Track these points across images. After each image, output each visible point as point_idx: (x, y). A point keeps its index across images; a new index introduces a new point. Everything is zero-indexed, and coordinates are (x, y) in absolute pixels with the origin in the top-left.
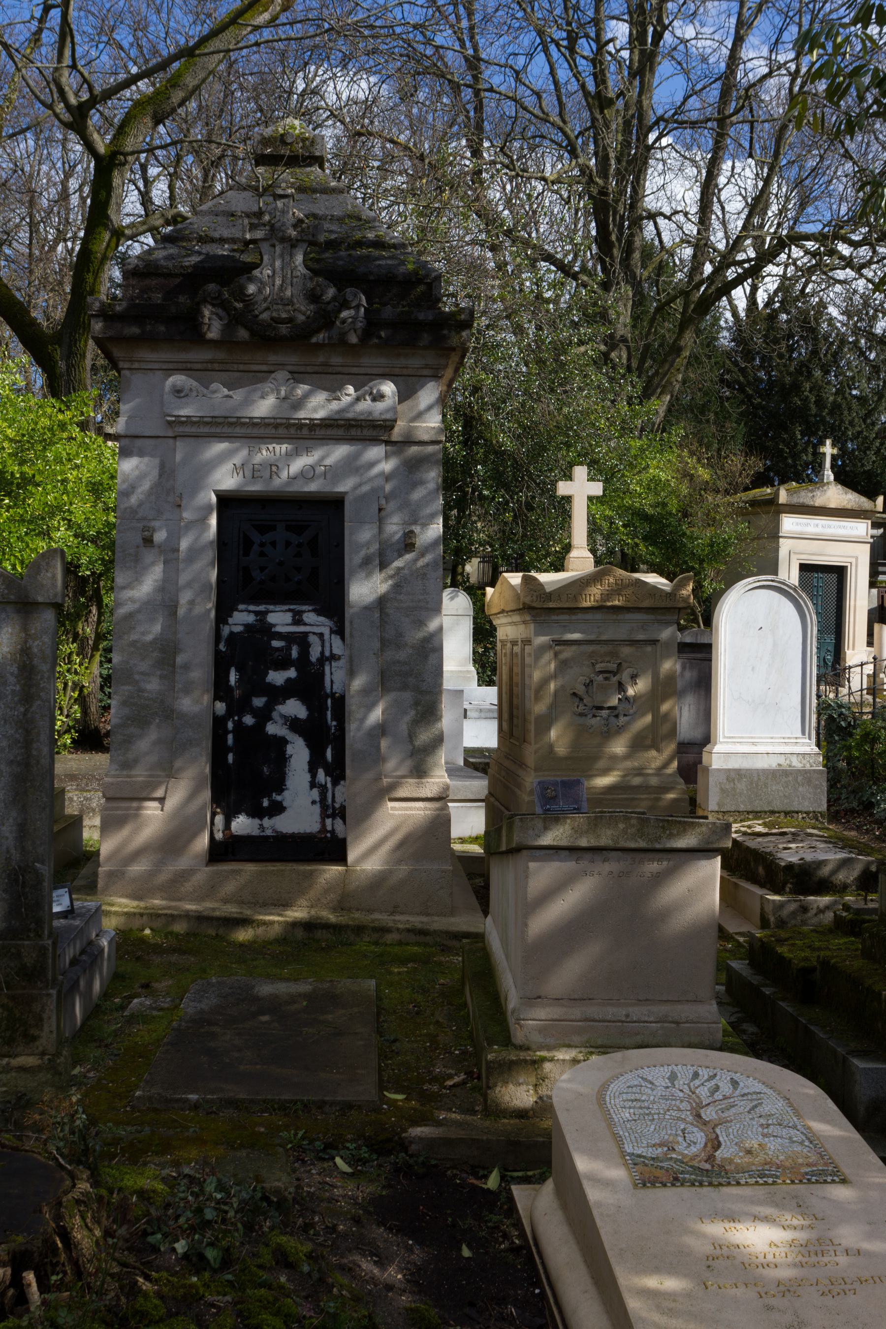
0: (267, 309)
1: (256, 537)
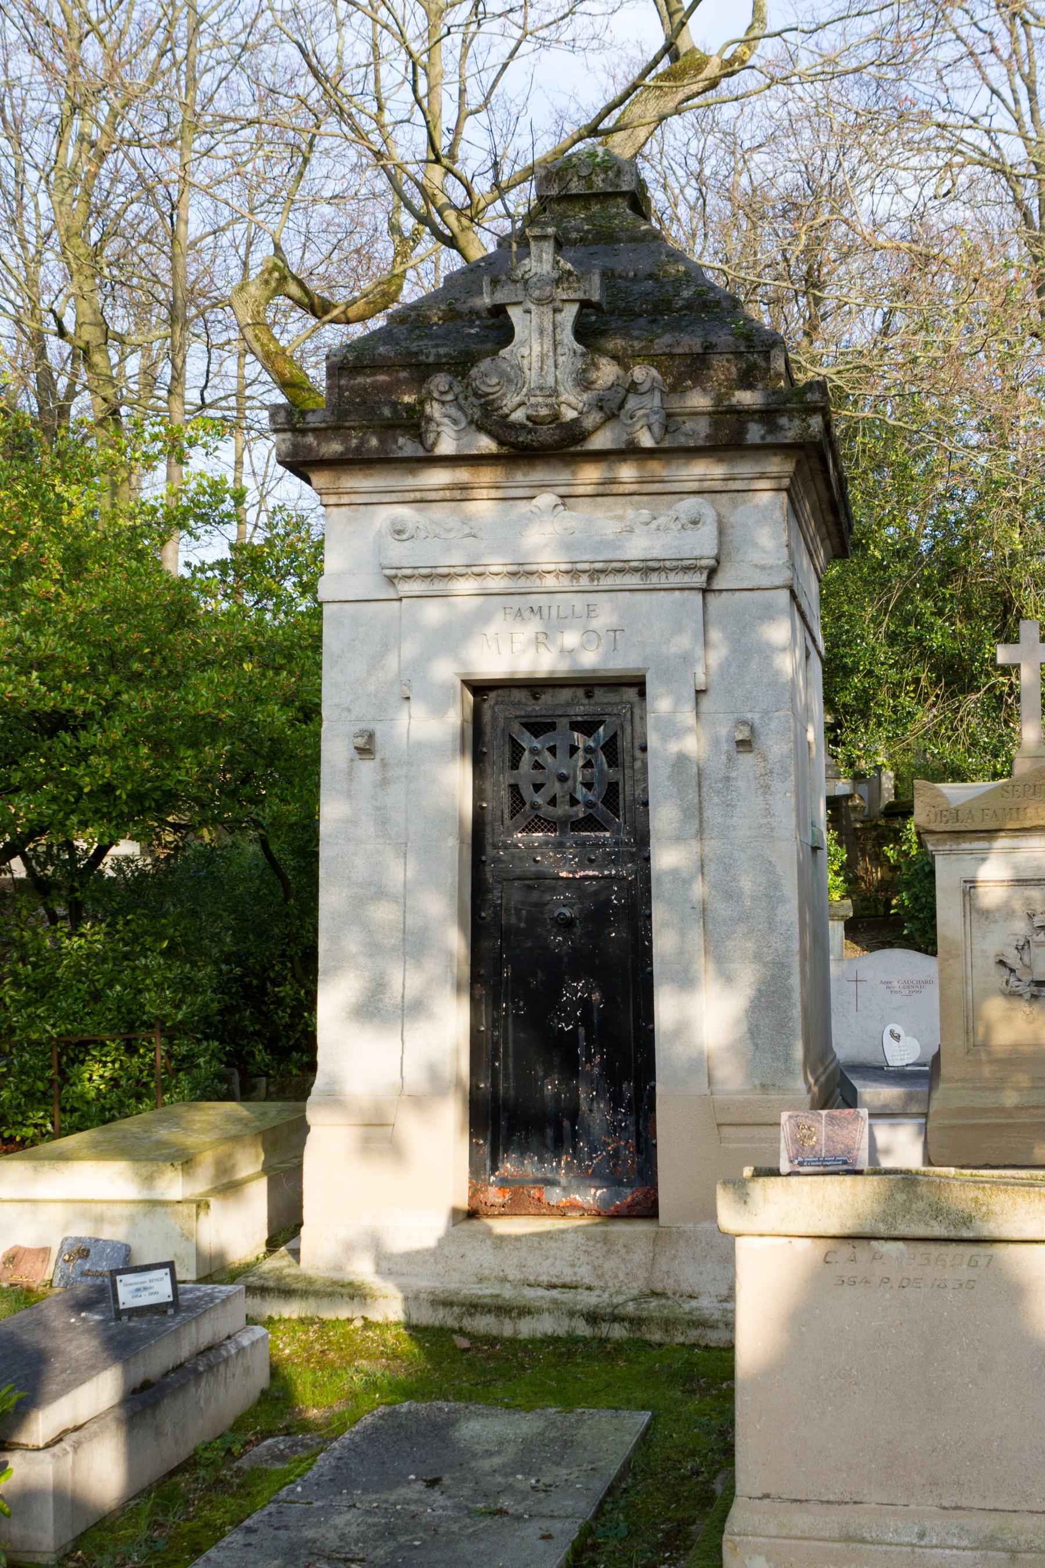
1: (527, 741)
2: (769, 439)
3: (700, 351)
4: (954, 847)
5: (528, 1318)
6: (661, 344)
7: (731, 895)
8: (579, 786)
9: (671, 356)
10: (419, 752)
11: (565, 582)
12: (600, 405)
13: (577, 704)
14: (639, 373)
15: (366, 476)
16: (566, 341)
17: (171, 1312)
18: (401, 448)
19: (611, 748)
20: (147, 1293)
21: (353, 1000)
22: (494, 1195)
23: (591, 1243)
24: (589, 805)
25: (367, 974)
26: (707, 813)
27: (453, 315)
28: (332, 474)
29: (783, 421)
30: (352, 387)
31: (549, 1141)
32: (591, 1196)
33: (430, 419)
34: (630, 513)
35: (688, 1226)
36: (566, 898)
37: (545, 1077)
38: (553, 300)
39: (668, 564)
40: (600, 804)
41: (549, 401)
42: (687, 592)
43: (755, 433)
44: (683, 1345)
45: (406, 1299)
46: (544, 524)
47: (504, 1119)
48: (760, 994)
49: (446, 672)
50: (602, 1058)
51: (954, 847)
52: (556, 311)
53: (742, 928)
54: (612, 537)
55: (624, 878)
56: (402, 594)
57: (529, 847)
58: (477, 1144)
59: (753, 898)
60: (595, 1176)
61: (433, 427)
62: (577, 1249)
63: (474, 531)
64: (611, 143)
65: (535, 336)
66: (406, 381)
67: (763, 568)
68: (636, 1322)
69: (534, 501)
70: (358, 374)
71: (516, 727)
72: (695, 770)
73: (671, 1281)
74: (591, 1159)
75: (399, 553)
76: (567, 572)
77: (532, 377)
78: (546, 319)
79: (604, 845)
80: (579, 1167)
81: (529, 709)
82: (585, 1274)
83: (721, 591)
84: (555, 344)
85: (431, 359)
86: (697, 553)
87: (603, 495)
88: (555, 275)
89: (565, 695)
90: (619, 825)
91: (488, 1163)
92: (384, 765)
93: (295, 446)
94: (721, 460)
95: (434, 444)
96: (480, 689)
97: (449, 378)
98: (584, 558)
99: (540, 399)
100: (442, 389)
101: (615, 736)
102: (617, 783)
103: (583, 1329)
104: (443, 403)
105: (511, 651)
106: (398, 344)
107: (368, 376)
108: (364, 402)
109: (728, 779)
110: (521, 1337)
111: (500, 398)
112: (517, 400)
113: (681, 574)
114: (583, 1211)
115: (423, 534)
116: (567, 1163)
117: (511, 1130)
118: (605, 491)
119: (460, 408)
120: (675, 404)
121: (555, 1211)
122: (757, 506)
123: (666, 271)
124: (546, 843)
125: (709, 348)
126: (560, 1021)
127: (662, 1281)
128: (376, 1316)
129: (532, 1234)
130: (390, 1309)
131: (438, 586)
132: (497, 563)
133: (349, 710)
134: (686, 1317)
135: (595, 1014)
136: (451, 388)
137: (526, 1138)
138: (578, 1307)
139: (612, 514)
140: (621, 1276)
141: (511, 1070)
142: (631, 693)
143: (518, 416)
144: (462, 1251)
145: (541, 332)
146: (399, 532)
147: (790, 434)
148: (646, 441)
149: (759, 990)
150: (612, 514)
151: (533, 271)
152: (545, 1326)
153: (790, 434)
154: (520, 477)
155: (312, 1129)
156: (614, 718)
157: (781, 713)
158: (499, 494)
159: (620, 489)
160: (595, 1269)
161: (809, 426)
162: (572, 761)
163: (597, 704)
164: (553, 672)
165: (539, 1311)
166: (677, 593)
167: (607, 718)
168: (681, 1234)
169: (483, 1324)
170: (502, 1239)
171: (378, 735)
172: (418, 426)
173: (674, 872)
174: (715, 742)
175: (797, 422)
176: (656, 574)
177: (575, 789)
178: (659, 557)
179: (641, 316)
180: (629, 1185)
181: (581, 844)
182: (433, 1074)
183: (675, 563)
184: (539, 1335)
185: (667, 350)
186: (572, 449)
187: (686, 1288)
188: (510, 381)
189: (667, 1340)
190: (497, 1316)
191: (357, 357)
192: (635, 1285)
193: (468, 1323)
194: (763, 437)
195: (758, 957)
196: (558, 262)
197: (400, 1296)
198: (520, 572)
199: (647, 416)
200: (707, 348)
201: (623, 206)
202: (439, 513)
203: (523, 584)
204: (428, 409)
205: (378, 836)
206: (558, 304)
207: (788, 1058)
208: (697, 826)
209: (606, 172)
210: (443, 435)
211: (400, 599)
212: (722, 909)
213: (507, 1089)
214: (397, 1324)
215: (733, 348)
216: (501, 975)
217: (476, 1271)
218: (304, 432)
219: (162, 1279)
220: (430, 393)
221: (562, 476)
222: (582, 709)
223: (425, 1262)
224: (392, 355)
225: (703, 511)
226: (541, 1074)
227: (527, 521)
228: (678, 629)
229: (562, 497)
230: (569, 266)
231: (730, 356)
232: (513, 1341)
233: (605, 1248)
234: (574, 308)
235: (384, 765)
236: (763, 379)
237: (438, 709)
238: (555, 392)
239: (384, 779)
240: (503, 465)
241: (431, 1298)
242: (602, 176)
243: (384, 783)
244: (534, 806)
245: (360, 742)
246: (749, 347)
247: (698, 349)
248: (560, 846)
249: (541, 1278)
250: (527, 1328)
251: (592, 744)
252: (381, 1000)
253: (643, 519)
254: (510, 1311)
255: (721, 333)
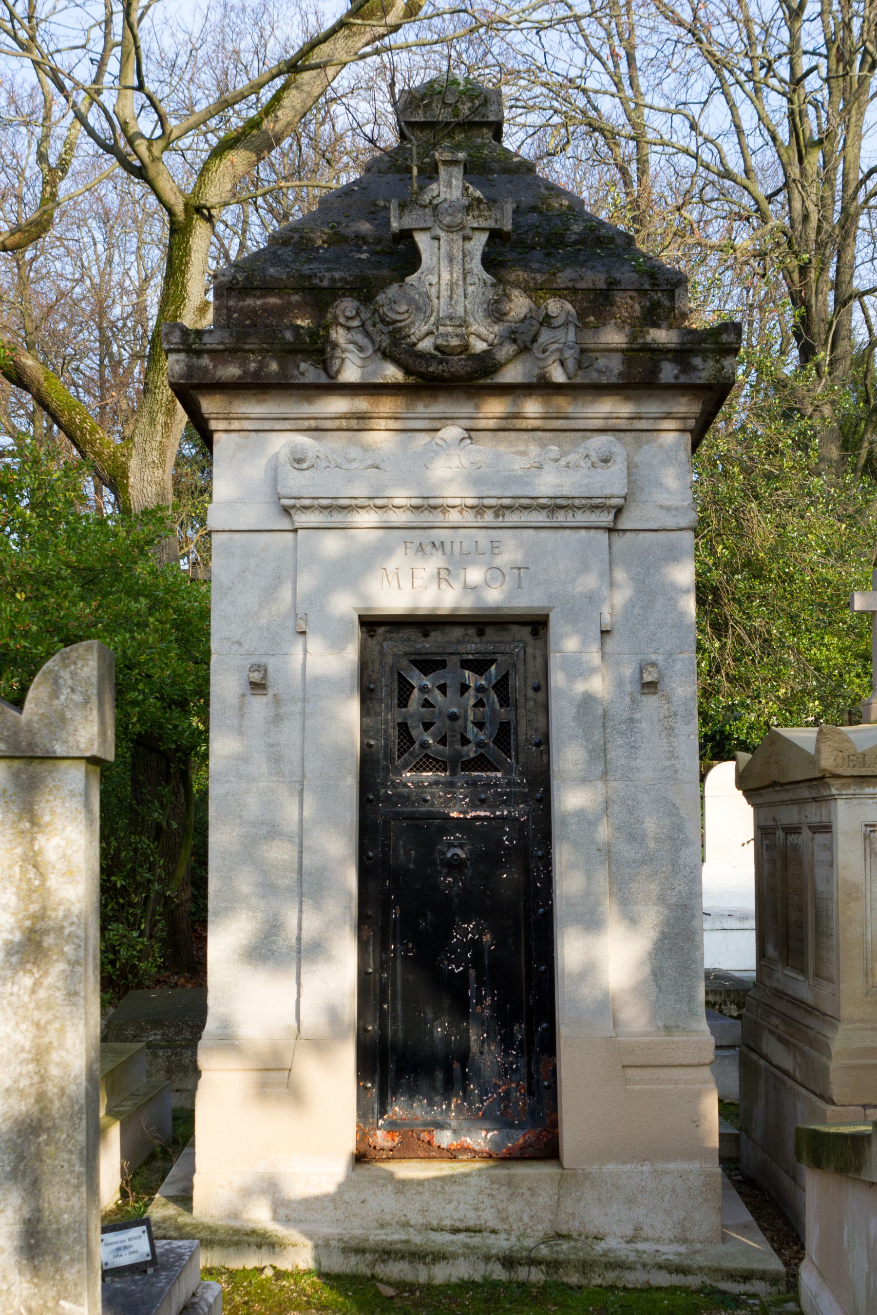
0: (430, 333)
1: (416, 679)
2: (683, 379)
3: (604, 287)
4: (858, 791)
5: (443, 1264)
6: (564, 278)
7: (634, 837)
8: (470, 726)
9: (574, 290)
10: (311, 689)
11: (469, 518)
12: (512, 336)
13: (468, 642)
14: (554, 306)
15: (259, 402)
16: (475, 270)
17: (150, 1271)
18: (302, 374)
19: (502, 686)
20: (127, 1252)
21: (245, 942)
22: (381, 1138)
23: (496, 1186)
24: (480, 744)
25: (259, 915)
26: (611, 755)
27: (337, 239)
28: (223, 398)
29: (697, 361)
30: (242, 308)
31: (439, 1084)
32: (481, 1139)
33: (335, 345)
34: (534, 450)
35: (594, 1168)
36: (456, 838)
37: (434, 1020)
38: (464, 228)
39: (577, 502)
40: (491, 744)
41: (459, 331)
42: (592, 532)
43: (668, 372)
44: (600, 1286)
45: (316, 1247)
46: (454, 458)
47: (392, 1064)
48: (664, 936)
49: (345, 606)
50: (493, 999)
51: (858, 791)
52: (467, 238)
53: (646, 870)
54: (520, 473)
55: (517, 819)
56: (297, 525)
57: (419, 785)
58: (365, 1088)
59: (656, 839)
60: (487, 1118)
61: (338, 353)
62: (481, 1192)
63: (378, 463)
64: (300, 80)
65: (444, 263)
66: (298, 305)
67: (668, 509)
68: (553, 1265)
69: (440, 434)
70: (247, 295)
71: (404, 663)
72: (600, 712)
73: (576, 1223)
74: (482, 1102)
75: (296, 483)
76: (472, 508)
77: (442, 307)
78: (455, 246)
79: (496, 785)
80: (469, 1109)
81: (419, 646)
82: (489, 1217)
83: (625, 531)
84: (465, 274)
85: (325, 283)
86: (607, 492)
87: (504, 430)
88: (465, 202)
89: (457, 633)
90: (510, 765)
91: (376, 1106)
92: (277, 700)
93: (190, 368)
94: (628, 398)
95: (338, 372)
96: (371, 624)
97: (356, 303)
98: (493, 494)
99: (450, 329)
100: (348, 314)
101: (506, 676)
102: (508, 723)
103: (499, 1273)
104: (348, 329)
105: (410, 587)
106: (287, 266)
107: (258, 298)
108: (254, 325)
109: (631, 720)
110: (437, 1282)
111: (408, 326)
112: (425, 329)
113: (588, 513)
114: (475, 1155)
115: (323, 464)
116: (457, 1106)
117: (400, 1073)
118: (509, 425)
119: (367, 334)
120: (589, 340)
121: (445, 1153)
122: (661, 446)
123: (549, 205)
124: (436, 783)
125: (613, 285)
126: (451, 962)
127: (567, 1223)
128: (284, 1265)
129: (436, 1179)
130: (300, 1257)
131: (337, 518)
132: (401, 496)
133: (240, 644)
134: (604, 1259)
135: (486, 956)
136: (358, 314)
137: (415, 1082)
138: (494, 1252)
139: (513, 450)
140: (526, 1219)
141: (400, 1012)
142: (525, 633)
143: (426, 345)
144: (362, 1196)
145: (451, 260)
146: (299, 461)
147: (704, 374)
148: (558, 376)
149: (663, 933)
150: (513, 450)
151: (442, 197)
152: (460, 1271)
153: (704, 374)
154: (420, 409)
155: (203, 1074)
156: (505, 657)
157: (685, 656)
158: (398, 425)
159: (523, 424)
160: (499, 1212)
161: (723, 368)
162: (462, 700)
163: (488, 642)
164: (456, 609)
165: (454, 1256)
166: (583, 532)
167: (499, 657)
168: (586, 1176)
169: (397, 1270)
170: (403, 1185)
171: (270, 669)
172: (322, 352)
173: (580, 813)
174: (620, 683)
175: (711, 363)
176: (562, 512)
177: (465, 728)
178: (568, 494)
179: (534, 248)
180: (521, 1126)
181: (473, 784)
182: (333, 1015)
183: (584, 501)
184: (454, 1280)
185: (570, 285)
186: (482, 381)
187: (591, 1229)
188: (418, 309)
189: (584, 1282)
190: (411, 1262)
191: (247, 278)
192: (540, 1227)
193: (381, 1270)
194: (677, 377)
195: (661, 899)
196: (467, 189)
197: (310, 1244)
198: (428, 506)
199: (561, 351)
200: (611, 284)
201: (488, 133)
202: (335, 443)
203: (426, 518)
204: (333, 335)
205: (271, 774)
206: (468, 232)
207: (691, 1000)
208: (602, 768)
209: (472, 101)
210: (347, 361)
211: (295, 531)
212: (627, 851)
213: (395, 1032)
214: (309, 1272)
215: (637, 286)
216: (389, 915)
217: (381, 1216)
218: (199, 353)
219: (140, 1237)
220: (336, 317)
221: (466, 409)
222: (473, 647)
223: (324, 1208)
224: (284, 277)
225: (614, 449)
226: (430, 1016)
227: (433, 453)
228: (585, 568)
229: (467, 430)
230: (478, 194)
231: (634, 294)
232: (429, 1288)
233: (510, 1192)
234: (484, 237)
235: (277, 700)
236: (667, 318)
237: (336, 645)
238: (464, 323)
239: (277, 715)
240: (405, 395)
241: (342, 1245)
242: (469, 105)
243: (277, 719)
244: (424, 745)
245: (256, 677)
246: (653, 285)
247: (602, 285)
248: (451, 785)
249: (444, 1223)
250: (441, 1274)
251: (483, 682)
252: (275, 942)
253: (552, 455)
254: (424, 1257)
255: (623, 270)
